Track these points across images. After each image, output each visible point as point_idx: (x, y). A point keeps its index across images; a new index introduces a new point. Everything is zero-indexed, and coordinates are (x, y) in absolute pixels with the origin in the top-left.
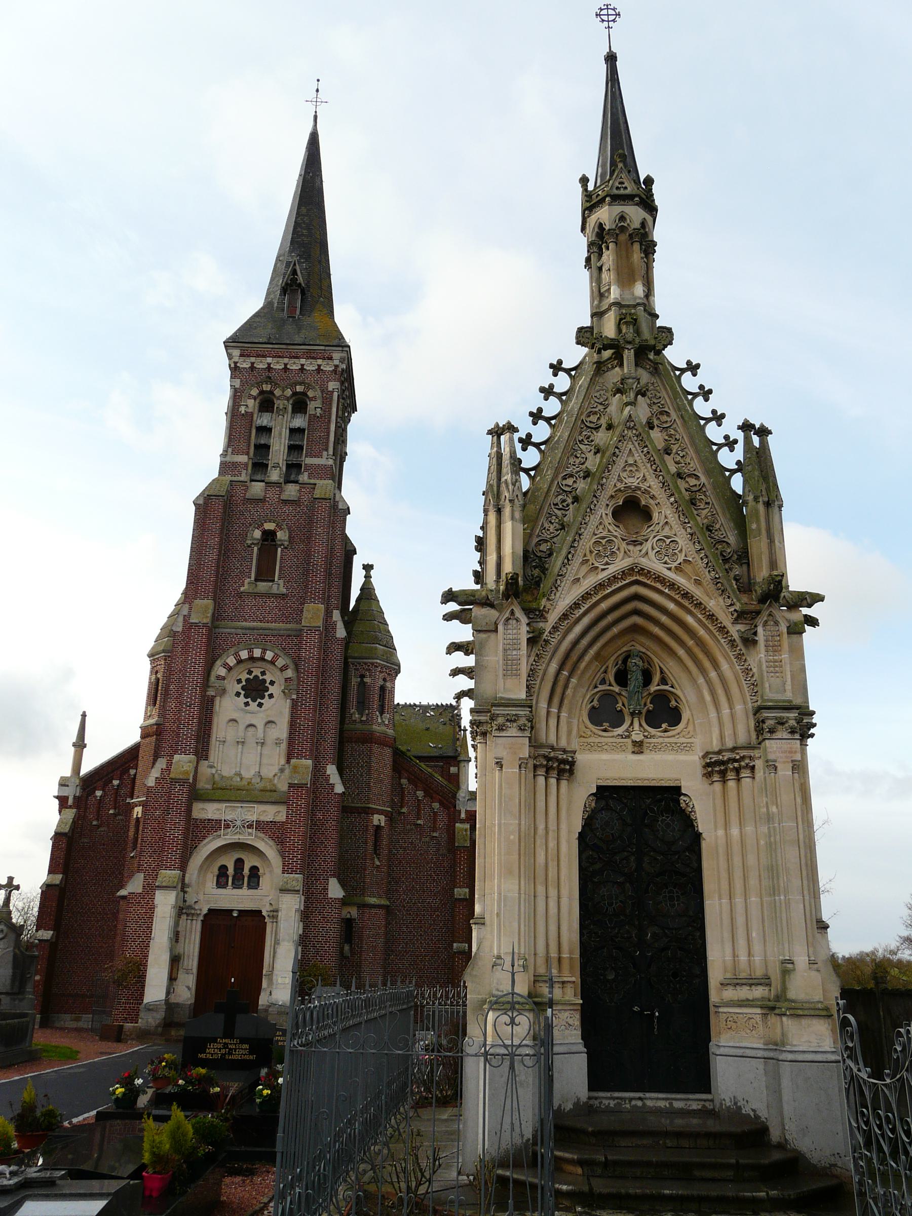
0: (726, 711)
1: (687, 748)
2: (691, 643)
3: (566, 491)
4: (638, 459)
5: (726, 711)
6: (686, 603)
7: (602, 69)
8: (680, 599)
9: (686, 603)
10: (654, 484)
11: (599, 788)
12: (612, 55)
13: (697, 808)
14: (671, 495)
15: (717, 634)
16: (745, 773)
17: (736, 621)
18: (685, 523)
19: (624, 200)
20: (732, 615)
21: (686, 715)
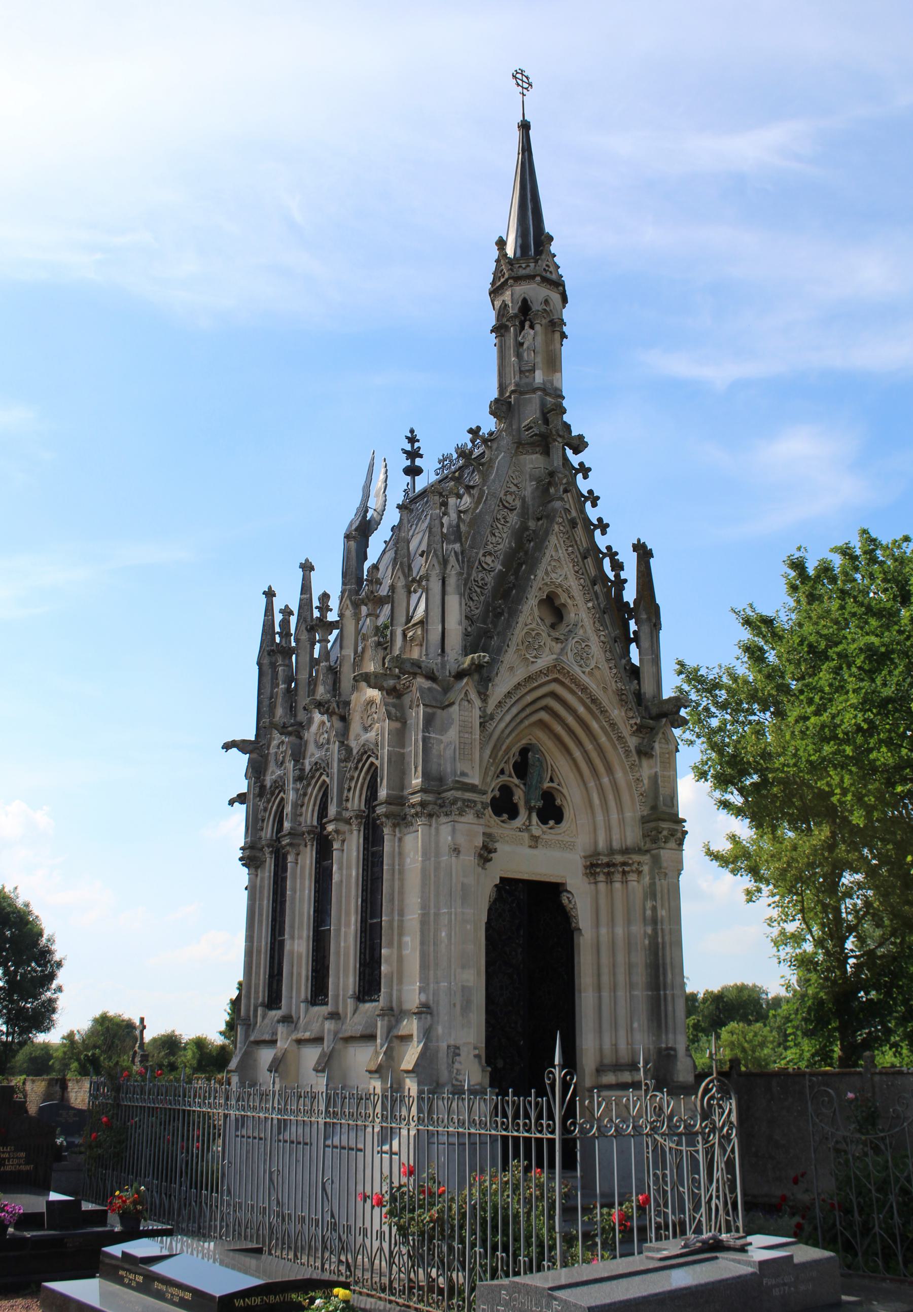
0: (614, 816)
1: (569, 846)
2: (589, 747)
3: (486, 570)
4: (561, 555)
5: (614, 816)
6: (593, 707)
7: (515, 135)
8: (589, 704)
9: (593, 707)
10: (574, 585)
11: (502, 879)
12: (526, 125)
13: (579, 905)
14: (590, 600)
15: (616, 742)
16: (632, 877)
17: (634, 733)
18: (599, 630)
19: (550, 285)
20: (632, 727)
21: (568, 814)
